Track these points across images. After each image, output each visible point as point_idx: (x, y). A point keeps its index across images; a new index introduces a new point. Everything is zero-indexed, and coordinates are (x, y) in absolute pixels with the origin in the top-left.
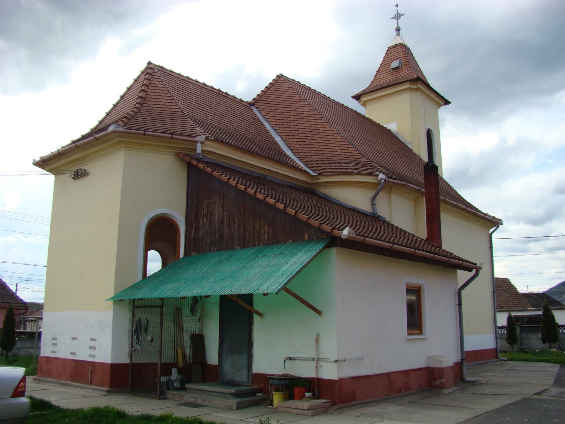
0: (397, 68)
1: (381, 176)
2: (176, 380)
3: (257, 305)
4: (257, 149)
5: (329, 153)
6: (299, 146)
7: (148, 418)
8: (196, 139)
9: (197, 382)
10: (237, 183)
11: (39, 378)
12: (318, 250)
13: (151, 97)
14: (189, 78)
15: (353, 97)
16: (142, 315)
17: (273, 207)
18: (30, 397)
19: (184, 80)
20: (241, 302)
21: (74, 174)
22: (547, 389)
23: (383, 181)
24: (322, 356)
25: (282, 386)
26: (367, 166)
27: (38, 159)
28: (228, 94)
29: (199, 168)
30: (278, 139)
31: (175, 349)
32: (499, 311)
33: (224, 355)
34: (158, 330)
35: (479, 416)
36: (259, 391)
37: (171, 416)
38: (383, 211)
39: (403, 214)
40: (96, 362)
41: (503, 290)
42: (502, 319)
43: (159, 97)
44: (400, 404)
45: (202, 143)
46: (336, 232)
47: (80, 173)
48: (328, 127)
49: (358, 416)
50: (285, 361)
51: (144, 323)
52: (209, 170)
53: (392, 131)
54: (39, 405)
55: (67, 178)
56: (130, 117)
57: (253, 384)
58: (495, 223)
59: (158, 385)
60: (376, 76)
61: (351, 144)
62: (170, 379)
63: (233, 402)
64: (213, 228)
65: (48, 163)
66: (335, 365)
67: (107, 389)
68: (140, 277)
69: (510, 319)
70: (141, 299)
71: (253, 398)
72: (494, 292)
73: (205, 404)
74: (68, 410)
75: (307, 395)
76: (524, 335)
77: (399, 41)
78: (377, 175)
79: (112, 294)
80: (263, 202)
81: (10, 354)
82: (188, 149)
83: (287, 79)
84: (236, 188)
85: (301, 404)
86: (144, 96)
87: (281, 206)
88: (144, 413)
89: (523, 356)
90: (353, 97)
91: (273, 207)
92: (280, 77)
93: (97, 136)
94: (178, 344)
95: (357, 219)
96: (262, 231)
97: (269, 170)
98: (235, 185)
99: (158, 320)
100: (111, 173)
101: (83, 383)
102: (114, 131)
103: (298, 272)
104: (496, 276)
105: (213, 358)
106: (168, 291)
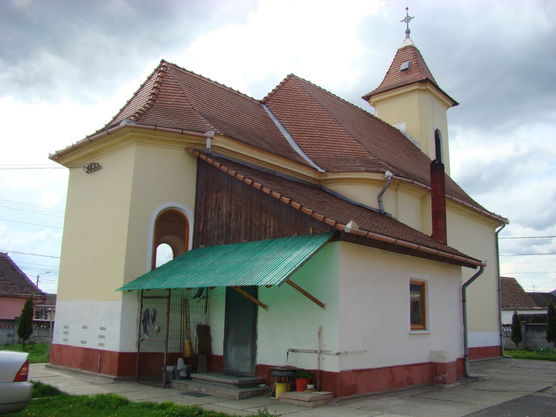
0: (407, 69)
1: (388, 173)
2: (181, 369)
3: (262, 298)
4: (265, 145)
5: (337, 150)
6: (308, 143)
7: (149, 406)
8: (206, 134)
9: (202, 372)
10: (244, 177)
11: (51, 365)
12: (322, 244)
13: (163, 93)
14: (202, 77)
15: (364, 98)
16: (150, 305)
17: (279, 201)
18: (31, 382)
19: (196, 78)
20: (246, 294)
21: (88, 168)
22: (550, 387)
23: (389, 178)
24: (324, 349)
25: (285, 377)
26: (374, 164)
27: (53, 153)
28: (239, 93)
29: (208, 163)
30: (287, 136)
31: (182, 339)
32: (505, 310)
33: (229, 346)
34: (166, 320)
35: (480, 411)
36: (262, 382)
37: (171, 404)
38: (389, 208)
39: (410, 211)
40: (104, 351)
41: (509, 290)
42: (507, 318)
43: (171, 94)
44: (401, 398)
45: (212, 138)
46: (340, 226)
47: (93, 167)
48: (337, 125)
49: (358, 409)
50: (288, 353)
51: (151, 313)
52: (217, 164)
53: (401, 131)
54: (45, 392)
55: (81, 171)
56: (142, 113)
57: (256, 374)
58: (501, 222)
59: (164, 374)
60: (386, 77)
61: (359, 143)
62: (176, 369)
63: (236, 392)
64: (221, 222)
65: (63, 157)
66: (337, 357)
67: (115, 377)
68: (149, 268)
69: (515, 317)
70: (149, 290)
71: (256, 389)
72: (499, 290)
73: (209, 393)
74: (74, 396)
75: (309, 386)
76: (529, 334)
77: (408, 43)
78: (384, 173)
79: (121, 285)
80: (269, 196)
81: (26, 342)
82: (197, 144)
83: (297, 79)
84: (243, 182)
85: (303, 395)
86: (156, 93)
87: (286, 200)
88: (147, 401)
89: (528, 354)
90: (364, 98)
91: (278, 201)
92: (291, 76)
93: (109, 131)
94: (184, 333)
95: (363, 215)
96: (268, 225)
97: (278, 166)
98: (242, 180)
99: (166, 310)
100: (122, 167)
101: (93, 371)
102: (126, 126)
103: (301, 265)
104: (501, 275)
105: (218, 349)
106: (174, 282)
